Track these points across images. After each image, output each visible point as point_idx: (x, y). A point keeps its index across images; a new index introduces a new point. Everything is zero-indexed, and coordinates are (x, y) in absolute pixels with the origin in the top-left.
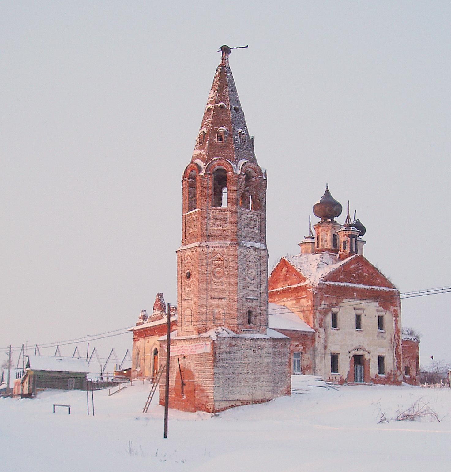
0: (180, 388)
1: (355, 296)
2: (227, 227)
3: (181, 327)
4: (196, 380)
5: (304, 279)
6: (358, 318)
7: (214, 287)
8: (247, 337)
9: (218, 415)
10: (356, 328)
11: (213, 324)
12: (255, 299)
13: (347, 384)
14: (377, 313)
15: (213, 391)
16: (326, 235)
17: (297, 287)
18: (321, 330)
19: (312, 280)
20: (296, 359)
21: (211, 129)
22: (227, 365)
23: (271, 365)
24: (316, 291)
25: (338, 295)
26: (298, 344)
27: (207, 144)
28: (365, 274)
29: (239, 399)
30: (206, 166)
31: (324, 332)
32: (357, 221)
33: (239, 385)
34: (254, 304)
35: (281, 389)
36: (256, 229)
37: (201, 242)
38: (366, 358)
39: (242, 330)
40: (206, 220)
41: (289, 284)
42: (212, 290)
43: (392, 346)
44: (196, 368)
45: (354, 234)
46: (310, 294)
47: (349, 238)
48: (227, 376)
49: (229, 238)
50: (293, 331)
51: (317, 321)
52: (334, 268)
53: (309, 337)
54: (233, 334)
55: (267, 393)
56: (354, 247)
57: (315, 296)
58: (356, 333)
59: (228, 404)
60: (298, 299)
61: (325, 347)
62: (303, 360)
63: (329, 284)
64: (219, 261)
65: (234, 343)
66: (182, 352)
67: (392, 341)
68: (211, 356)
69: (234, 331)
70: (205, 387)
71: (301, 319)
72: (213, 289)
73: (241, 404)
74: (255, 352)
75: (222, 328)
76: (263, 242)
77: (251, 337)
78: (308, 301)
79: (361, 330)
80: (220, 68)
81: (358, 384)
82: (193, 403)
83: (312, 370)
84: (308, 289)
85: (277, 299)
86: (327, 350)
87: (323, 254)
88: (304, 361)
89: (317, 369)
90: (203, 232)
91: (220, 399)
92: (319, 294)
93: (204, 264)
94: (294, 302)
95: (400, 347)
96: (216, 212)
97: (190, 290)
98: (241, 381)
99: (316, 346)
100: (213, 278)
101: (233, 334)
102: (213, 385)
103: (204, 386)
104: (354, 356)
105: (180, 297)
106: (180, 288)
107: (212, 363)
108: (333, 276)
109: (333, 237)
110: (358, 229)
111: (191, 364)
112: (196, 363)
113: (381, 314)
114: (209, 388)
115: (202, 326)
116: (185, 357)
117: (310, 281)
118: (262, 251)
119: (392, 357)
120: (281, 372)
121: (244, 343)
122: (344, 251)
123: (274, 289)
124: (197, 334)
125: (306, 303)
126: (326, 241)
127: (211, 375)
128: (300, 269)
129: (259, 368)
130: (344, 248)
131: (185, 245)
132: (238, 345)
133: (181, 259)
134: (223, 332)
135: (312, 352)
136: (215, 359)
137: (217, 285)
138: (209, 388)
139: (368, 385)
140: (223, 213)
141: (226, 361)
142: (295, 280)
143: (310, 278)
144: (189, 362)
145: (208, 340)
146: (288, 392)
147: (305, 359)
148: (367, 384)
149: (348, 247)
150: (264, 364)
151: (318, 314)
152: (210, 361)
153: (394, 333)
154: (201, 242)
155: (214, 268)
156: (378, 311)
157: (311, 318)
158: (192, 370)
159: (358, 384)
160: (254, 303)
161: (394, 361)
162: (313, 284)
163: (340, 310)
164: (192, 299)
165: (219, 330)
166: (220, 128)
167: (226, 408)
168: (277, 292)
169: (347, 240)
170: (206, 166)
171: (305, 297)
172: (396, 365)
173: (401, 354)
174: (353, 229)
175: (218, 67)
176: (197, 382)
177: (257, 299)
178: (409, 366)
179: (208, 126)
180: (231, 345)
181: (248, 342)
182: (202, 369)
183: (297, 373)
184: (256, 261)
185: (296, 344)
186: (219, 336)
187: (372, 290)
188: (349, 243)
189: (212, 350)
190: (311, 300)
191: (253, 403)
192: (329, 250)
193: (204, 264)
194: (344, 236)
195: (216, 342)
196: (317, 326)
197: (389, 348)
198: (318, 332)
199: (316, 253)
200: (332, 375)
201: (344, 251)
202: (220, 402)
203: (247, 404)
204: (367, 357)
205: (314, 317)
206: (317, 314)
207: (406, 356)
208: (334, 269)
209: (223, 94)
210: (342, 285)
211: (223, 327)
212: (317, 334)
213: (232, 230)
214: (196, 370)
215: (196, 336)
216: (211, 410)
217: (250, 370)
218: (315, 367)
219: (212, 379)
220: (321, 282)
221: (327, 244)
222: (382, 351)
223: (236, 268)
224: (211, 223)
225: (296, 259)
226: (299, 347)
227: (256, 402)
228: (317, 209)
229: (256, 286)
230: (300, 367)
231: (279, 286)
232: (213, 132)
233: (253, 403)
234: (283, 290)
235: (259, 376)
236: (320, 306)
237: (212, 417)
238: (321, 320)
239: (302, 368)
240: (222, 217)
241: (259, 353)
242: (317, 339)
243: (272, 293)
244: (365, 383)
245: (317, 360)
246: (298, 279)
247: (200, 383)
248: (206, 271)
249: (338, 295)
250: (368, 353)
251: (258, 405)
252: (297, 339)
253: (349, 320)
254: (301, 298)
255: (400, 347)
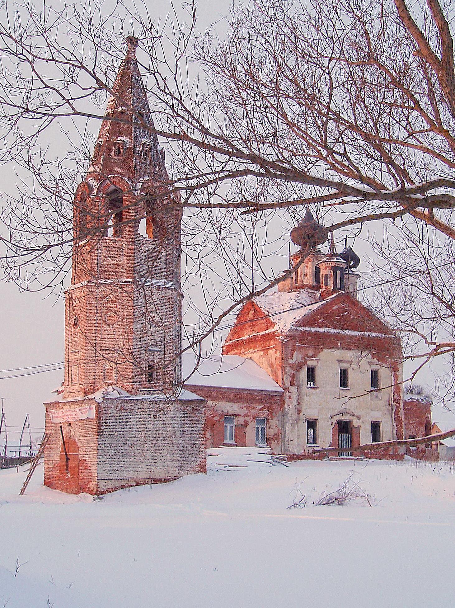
0: (64, 463)
1: (339, 344)
2: (123, 261)
3: (67, 387)
4: (80, 453)
5: (273, 325)
6: (344, 374)
7: (105, 337)
8: (144, 399)
9: (103, 498)
10: (341, 387)
11: (102, 383)
12: (156, 351)
13: (328, 458)
14: (369, 366)
15: (96, 468)
16: (306, 268)
17: (263, 335)
18: (293, 389)
19: (282, 325)
20: (260, 427)
21: (108, 139)
22: (116, 434)
23: (178, 434)
24: (285, 339)
25: (316, 344)
26: (261, 407)
27: (102, 159)
28: (352, 317)
29: (132, 477)
30: (98, 185)
31: (296, 392)
32: (348, 249)
33: (132, 459)
34: (156, 357)
35: (193, 464)
36: (161, 263)
37: (90, 281)
38: (354, 425)
39: (138, 390)
40: (97, 253)
41: (257, 331)
42: (102, 340)
43: (390, 408)
44: (80, 438)
45: (338, 266)
46: (279, 343)
47: (332, 271)
48: (116, 448)
49: (125, 274)
50: (255, 390)
51: (287, 378)
52: (311, 310)
53: (276, 398)
54: (126, 395)
55: (172, 469)
56: (339, 282)
57: (284, 345)
58: (341, 392)
59: (117, 484)
60: (265, 350)
61: (299, 412)
62: (269, 428)
63: (302, 330)
64: (112, 304)
65: (126, 406)
66: (67, 418)
67: (390, 402)
68: (95, 422)
69: (127, 391)
70: (89, 462)
71: (269, 375)
72: (103, 339)
73: (135, 484)
74: (155, 417)
75: (113, 388)
76: (169, 279)
77: (151, 399)
78: (276, 353)
79: (348, 388)
80: (124, 64)
81: (344, 459)
82: (77, 482)
83: (280, 440)
84: (277, 337)
85: (243, 350)
86: (302, 414)
87: (300, 292)
88: (271, 429)
89: (287, 439)
90: (93, 267)
91: (107, 477)
92: (290, 343)
93: (93, 308)
94: (262, 353)
95: (402, 411)
96: (109, 243)
97: (77, 340)
98: (136, 455)
99: (286, 410)
100: (104, 324)
101: (126, 395)
102: (97, 460)
103: (88, 460)
104: (339, 422)
105: (67, 349)
106: (67, 338)
107: (96, 431)
108: (309, 320)
109: (315, 270)
110: (343, 260)
111: (75, 433)
112: (80, 431)
113: (375, 367)
114: (92, 463)
115: (90, 385)
116: (70, 425)
117: (279, 326)
118: (168, 291)
119: (390, 423)
120: (192, 442)
121: (141, 406)
122: (326, 288)
123: (240, 337)
124: (83, 395)
125: (275, 355)
126: (305, 275)
127: (95, 447)
128: (269, 312)
129: (162, 438)
130: (327, 284)
131: (75, 284)
132: (133, 408)
133: (70, 300)
134: (113, 393)
135: (280, 417)
136: (99, 426)
137: (109, 333)
138: (92, 463)
139: (358, 459)
140: (118, 244)
141: (115, 429)
142: (263, 325)
143: (279, 322)
144: (74, 430)
145: (93, 402)
146: (203, 469)
147: (271, 427)
148: (355, 458)
149: (331, 283)
150: (168, 433)
151: (288, 368)
152: (94, 430)
153: (393, 393)
154: (90, 281)
155: (105, 312)
156: (370, 363)
157: (280, 373)
158: (77, 441)
159: (344, 459)
160: (157, 355)
161: (393, 429)
162: (283, 331)
163: (319, 363)
164: (79, 351)
165: (109, 390)
166: (118, 139)
167: (115, 489)
168: (243, 341)
169: (330, 273)
170: (98, 185)
171: (274, 347)
172: (396, 433)
173: (403, 419)
174: (337, 259)
175: (121, 63)
176: (81, 456)
177: (160, 351)
178: (415, 435)
179: (105, 136)
180: (122, 409)
181: (146, 405)
182: (86, 439)
183: (261, 445)
184: (159, 303)
185: (260, 407)
186: (105, 397)
187: (363, 337)
188: (332, 278)
189: (96, 415)
190: (280, 351)
191: (153, 482)
192: (310, 287)
193: (93, 308)
194: (326, 269)
195: (102, 405)
196: (287, 384)
197: (386, 412)
198: (289, 392)
199: (292, 290)
200: (307, 447)
201: (326, 288)
202: (106, 481)
203: (143, 484)
204: (356, 423)
205: (284, 373)
206: (288, 369)
207: (411, 422)
208: (311, 311)
209: (125, 96)
210: (320, 331)
211: (114, 387)
212: (287, 394)
213: (128, 265)
214: (80, 441)
215: (81, 397)
216: (95, 491)
217: (149, 440)
218: (285, 437)
219: (96, 452)
220: (293, 328)
221: (307, 279)
222: (376, 416)
223: (131, 311)
224: (103, 257)
225: (265, 299)
226: (263, 411)
227: (156, 481)
228: (295, 234)
229: (159, 334)
230: (265, 436)
231: (245, 334)
232: (110, 143)
233: (153, 482)
234: (249, 339)
235: (161, 448)
236: (292, 359)
237: (94, 500)
238: (293, 376)
239: (268, 438)
240: (116, 249)
241: (161, 419)
242: (287, 400)
243: (237, 343)
244: (353, 457)
245: (288, 428)
246: (266, 324)
247: (84, 457)
248: (95, 316)
249: (316, 344)
250: (356, 418)
251: (159, 485)
252: (259, 401)
253: (331, 375)
254: (269, 348)
255: (402, 411)
